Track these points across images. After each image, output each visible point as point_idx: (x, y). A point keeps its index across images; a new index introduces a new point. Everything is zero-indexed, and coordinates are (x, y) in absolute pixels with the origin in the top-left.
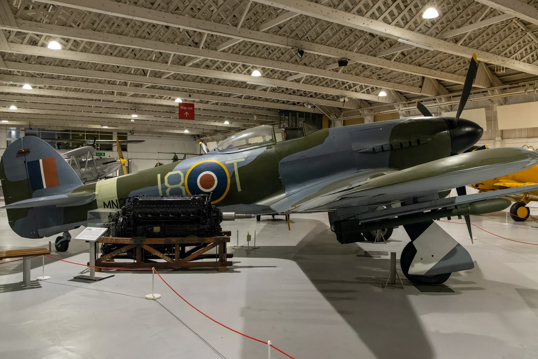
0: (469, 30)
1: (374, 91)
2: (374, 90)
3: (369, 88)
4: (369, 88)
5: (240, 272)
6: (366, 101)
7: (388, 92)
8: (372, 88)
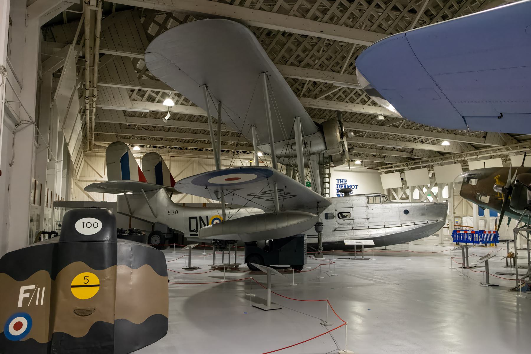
2: (438, 142)
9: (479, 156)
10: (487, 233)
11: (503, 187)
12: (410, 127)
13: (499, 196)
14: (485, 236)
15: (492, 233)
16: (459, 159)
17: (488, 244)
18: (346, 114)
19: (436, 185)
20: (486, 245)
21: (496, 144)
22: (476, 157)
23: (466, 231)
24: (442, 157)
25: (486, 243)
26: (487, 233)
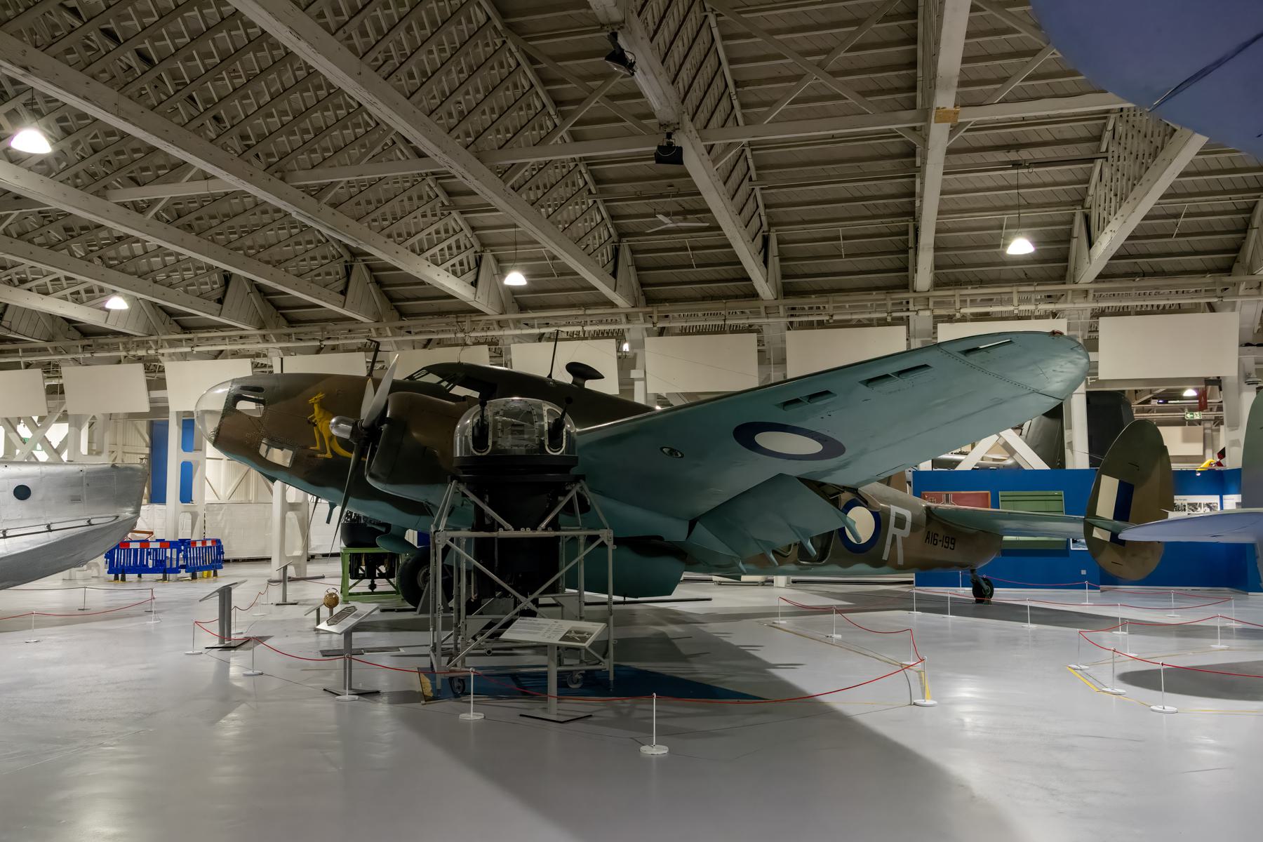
0: (343, 177)
1: (94, 298)
2: (91, 296)
3: (81, 288)
4: (81, 288)
5: (328, 521)
6: (69, 321)
7: (133, 301)
8: (89, 291)
9: (196, 349)
10: (199, 545)
11: (355, 425)
12: (29, 236)
13: (318, 447)
14: (192, 553)
15: (209, 544)
16: (141, 353)
17: (198, 574)
18: (622, 71)
19: (64, 417)
20: (194, 577)
21: (245, 322)
22: (189, 349)
23: (144, 543)
24: (86, 342)
25: (194, 572)
26: (199, 545)
